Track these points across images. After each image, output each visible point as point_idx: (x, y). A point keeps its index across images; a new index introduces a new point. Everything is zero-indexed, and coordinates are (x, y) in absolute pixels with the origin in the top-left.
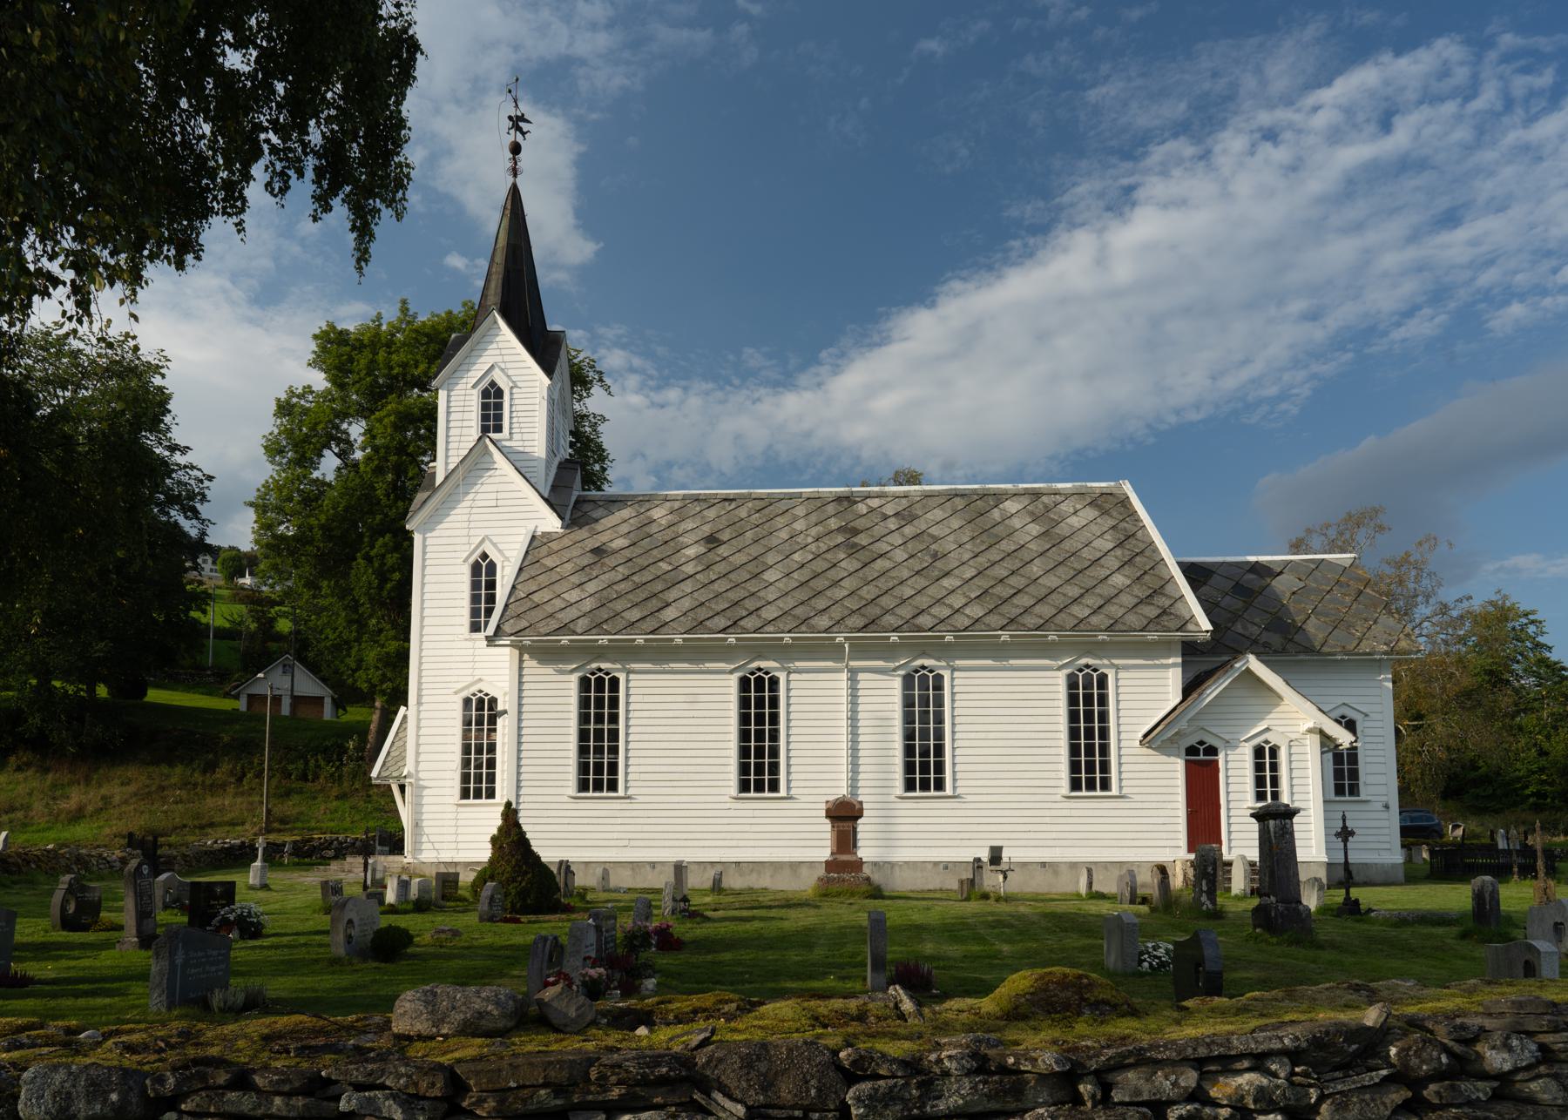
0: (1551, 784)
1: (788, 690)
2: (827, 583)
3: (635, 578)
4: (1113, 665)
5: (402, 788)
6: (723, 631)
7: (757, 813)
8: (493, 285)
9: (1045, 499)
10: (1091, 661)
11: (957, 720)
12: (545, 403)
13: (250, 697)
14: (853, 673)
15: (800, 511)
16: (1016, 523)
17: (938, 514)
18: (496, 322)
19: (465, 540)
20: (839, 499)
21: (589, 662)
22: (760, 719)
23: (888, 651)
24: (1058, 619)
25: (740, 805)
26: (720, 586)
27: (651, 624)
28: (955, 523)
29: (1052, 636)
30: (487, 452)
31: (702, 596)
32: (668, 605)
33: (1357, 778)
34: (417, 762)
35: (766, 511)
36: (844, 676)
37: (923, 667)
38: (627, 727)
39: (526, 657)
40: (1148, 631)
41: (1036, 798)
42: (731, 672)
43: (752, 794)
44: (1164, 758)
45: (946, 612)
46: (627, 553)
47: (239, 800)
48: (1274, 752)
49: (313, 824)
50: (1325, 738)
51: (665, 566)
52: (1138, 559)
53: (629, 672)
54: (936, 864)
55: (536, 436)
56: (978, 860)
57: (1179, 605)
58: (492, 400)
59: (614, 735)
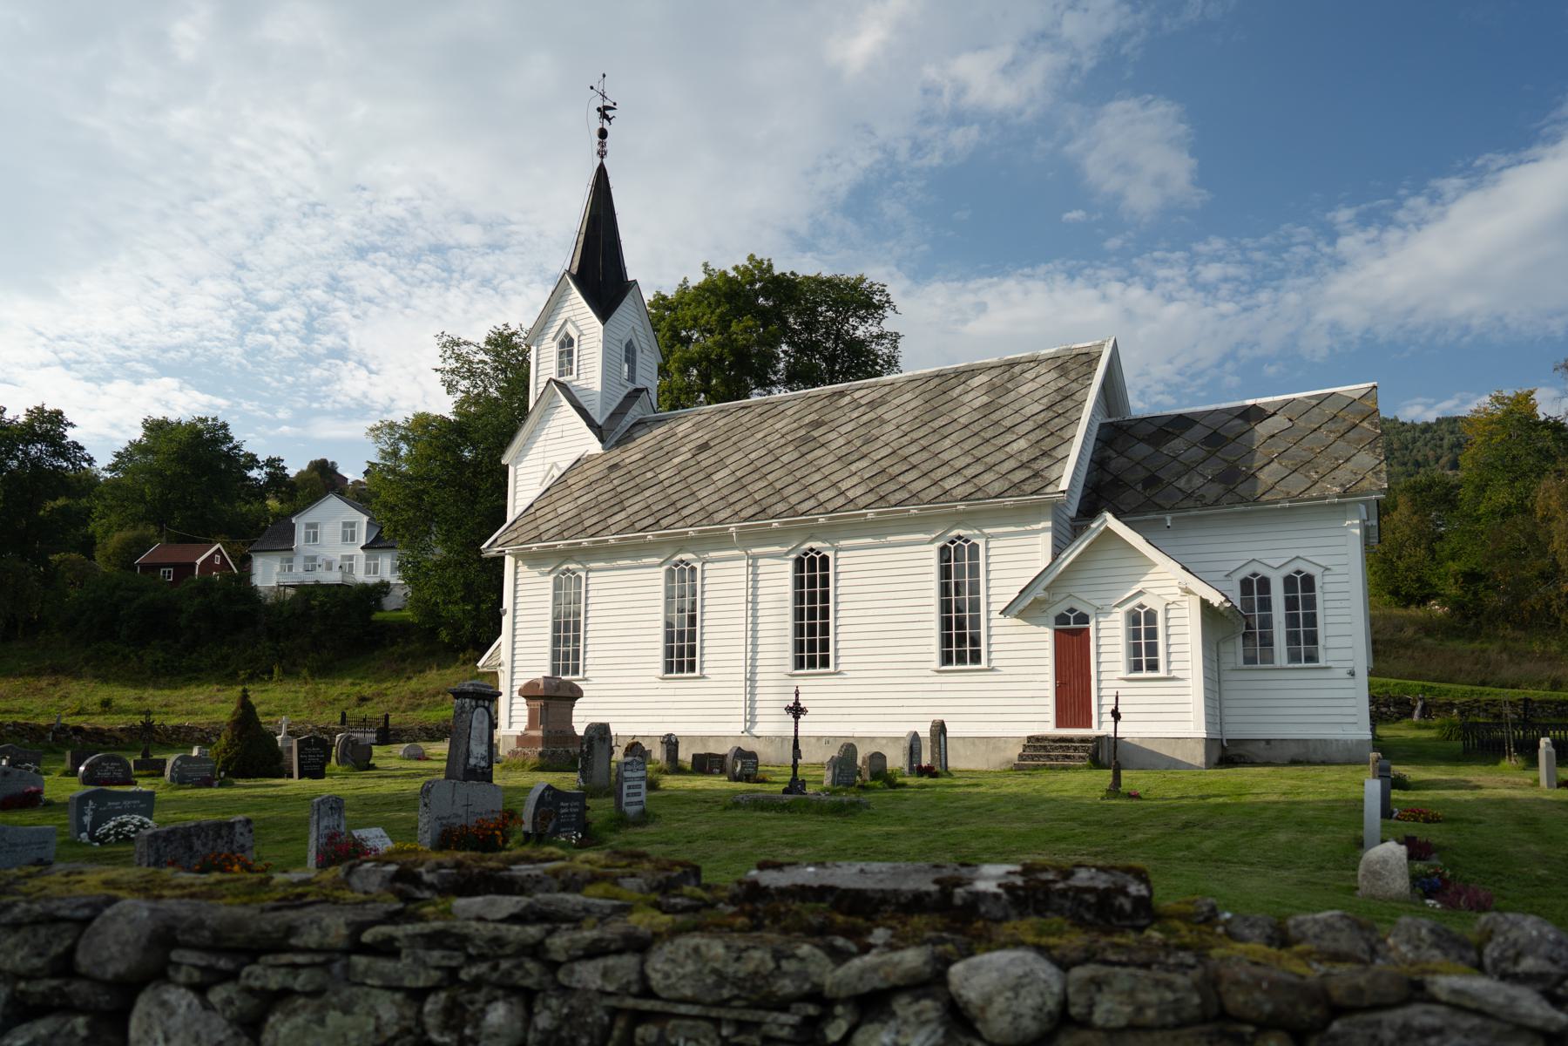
1: (987, 557)
4: (984, 535)
7: (678, 692)
10: (962, 532)
11: (840, 599)
21: (950, 530)
23: (766, 537)
29: (914, 511)
40: (1017, 500)
44: (1034, 628)
53: (988, 538)
54: (819, 738)
56: (915, 737)
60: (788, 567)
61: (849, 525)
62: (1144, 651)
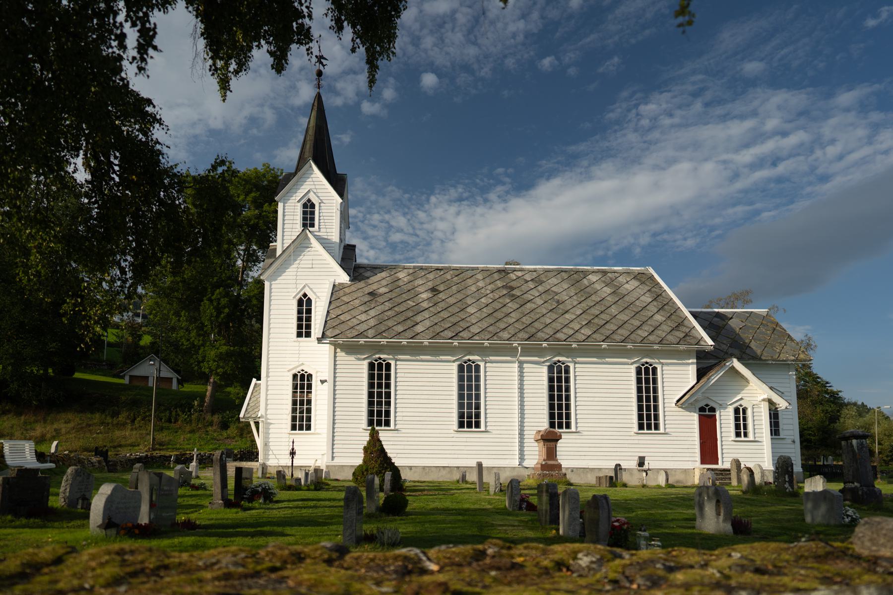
0: (815, 435)
1: (485, 372)
2: (503, 315)
3: (396, 309)
5: (257, 424)
6: (451, 338)
7: (468, 440)
8: (308, 146)
9: (609, 274)
10: (648, 360)
12: (339, 213)
13: (131, 377)
14: (521, 363)
15: (480, 276)
16: (597, 286)
17: (554, 281)
18: (311, 167)
19: (294, 286)
20: (499, 271)
21: (374, 354)
22: (470, 388)
23: (538, 351)
24: (632, 337)
25: (459, 435)
26: (444, 314)
27: (409, 333)
28: (565, 286)
29: (630, 346)
30: (307, 238)
31: (436, 319)
32: (417, 324)
33: (778, 426)
34: (266, 409)
35: (461, 276)
36: (516, 365)
37: (559, 361)
38: (396, 390)
39: (338, 350)
40: (677, 345)
41: (621, 433)
42: (454, 361)
43: (466, 429)
44: (688, 413)
45: (571, 332)
46: (389, 296)
47: (134, 432)
48: (744, 411)
49: (178, 446)
50: (771, 402)
51: (411, 303)
52: (666, 307)
53: (396, 360)
55: (334, 230)
57: (693, 331)
58: (309, 210)
59: (388, 395)
60: (544, 371)
61: (590, 351)
62: (741, 429)
